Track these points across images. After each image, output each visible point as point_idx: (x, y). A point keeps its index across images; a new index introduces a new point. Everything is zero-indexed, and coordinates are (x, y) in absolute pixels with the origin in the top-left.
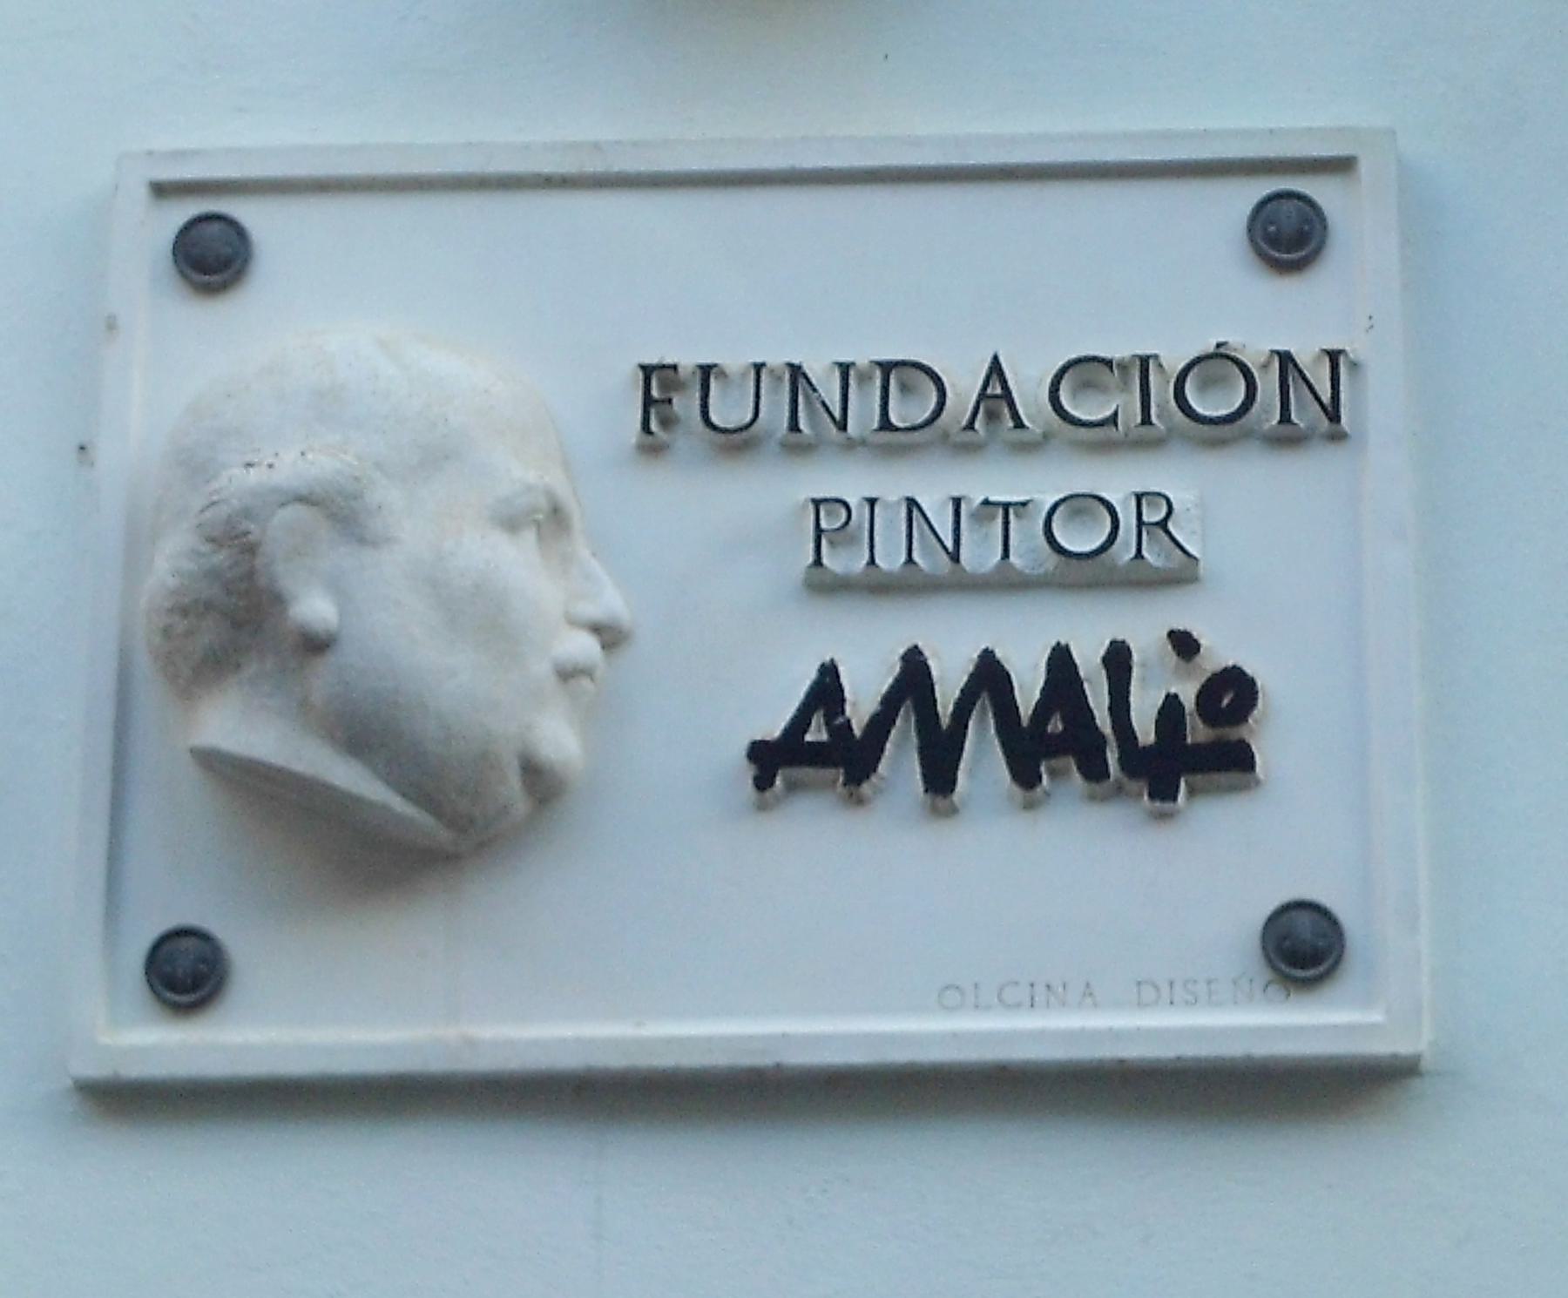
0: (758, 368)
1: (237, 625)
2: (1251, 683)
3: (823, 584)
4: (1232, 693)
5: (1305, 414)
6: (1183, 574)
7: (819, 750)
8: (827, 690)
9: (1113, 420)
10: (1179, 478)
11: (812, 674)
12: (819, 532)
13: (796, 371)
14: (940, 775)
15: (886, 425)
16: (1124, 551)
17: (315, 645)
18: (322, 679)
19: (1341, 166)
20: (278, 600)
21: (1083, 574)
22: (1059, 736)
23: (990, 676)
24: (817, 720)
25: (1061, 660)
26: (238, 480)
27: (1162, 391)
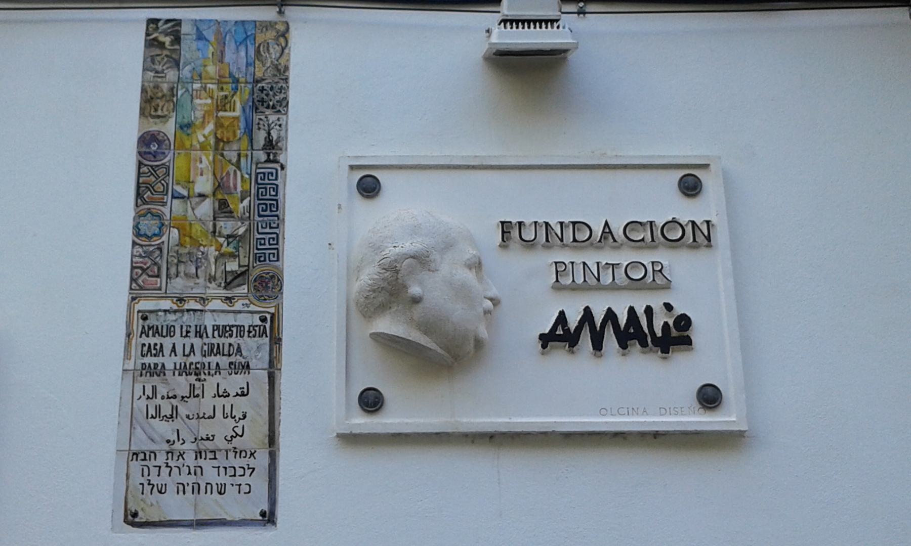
0: (536, 223)
1: (391, 295)
2: (689, 318)
3: (558, 287)
4: (684, 322)
5: (701, 239)
6: (667, 286)
7: (560, 336)
8: (562, 318)
9: (643, 240)
10: (664, 256)
11: (557, 314)
12: (557, 272)
13: (547, 224)
14: (598, 345)
15: (575, 240)
16: (649, 279)
17: (416, 300)
18: (418, 312)
19: (706, 166)
20: (405, 287)
21: (637, 285)
22: (632, 333)
23: (610, 315)
24: (560, 327)
25: (632, 310)
26: (391, 251)
27: (658, 233)
